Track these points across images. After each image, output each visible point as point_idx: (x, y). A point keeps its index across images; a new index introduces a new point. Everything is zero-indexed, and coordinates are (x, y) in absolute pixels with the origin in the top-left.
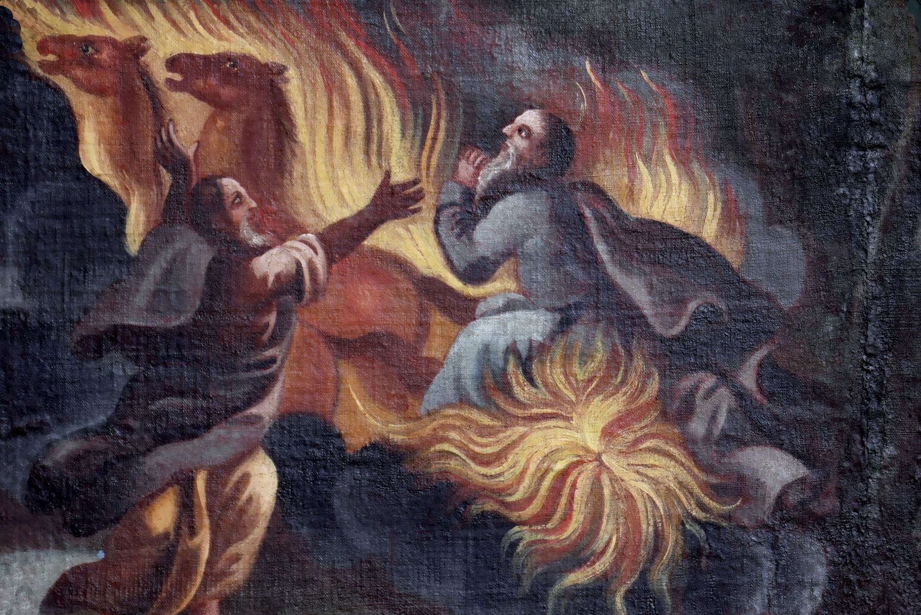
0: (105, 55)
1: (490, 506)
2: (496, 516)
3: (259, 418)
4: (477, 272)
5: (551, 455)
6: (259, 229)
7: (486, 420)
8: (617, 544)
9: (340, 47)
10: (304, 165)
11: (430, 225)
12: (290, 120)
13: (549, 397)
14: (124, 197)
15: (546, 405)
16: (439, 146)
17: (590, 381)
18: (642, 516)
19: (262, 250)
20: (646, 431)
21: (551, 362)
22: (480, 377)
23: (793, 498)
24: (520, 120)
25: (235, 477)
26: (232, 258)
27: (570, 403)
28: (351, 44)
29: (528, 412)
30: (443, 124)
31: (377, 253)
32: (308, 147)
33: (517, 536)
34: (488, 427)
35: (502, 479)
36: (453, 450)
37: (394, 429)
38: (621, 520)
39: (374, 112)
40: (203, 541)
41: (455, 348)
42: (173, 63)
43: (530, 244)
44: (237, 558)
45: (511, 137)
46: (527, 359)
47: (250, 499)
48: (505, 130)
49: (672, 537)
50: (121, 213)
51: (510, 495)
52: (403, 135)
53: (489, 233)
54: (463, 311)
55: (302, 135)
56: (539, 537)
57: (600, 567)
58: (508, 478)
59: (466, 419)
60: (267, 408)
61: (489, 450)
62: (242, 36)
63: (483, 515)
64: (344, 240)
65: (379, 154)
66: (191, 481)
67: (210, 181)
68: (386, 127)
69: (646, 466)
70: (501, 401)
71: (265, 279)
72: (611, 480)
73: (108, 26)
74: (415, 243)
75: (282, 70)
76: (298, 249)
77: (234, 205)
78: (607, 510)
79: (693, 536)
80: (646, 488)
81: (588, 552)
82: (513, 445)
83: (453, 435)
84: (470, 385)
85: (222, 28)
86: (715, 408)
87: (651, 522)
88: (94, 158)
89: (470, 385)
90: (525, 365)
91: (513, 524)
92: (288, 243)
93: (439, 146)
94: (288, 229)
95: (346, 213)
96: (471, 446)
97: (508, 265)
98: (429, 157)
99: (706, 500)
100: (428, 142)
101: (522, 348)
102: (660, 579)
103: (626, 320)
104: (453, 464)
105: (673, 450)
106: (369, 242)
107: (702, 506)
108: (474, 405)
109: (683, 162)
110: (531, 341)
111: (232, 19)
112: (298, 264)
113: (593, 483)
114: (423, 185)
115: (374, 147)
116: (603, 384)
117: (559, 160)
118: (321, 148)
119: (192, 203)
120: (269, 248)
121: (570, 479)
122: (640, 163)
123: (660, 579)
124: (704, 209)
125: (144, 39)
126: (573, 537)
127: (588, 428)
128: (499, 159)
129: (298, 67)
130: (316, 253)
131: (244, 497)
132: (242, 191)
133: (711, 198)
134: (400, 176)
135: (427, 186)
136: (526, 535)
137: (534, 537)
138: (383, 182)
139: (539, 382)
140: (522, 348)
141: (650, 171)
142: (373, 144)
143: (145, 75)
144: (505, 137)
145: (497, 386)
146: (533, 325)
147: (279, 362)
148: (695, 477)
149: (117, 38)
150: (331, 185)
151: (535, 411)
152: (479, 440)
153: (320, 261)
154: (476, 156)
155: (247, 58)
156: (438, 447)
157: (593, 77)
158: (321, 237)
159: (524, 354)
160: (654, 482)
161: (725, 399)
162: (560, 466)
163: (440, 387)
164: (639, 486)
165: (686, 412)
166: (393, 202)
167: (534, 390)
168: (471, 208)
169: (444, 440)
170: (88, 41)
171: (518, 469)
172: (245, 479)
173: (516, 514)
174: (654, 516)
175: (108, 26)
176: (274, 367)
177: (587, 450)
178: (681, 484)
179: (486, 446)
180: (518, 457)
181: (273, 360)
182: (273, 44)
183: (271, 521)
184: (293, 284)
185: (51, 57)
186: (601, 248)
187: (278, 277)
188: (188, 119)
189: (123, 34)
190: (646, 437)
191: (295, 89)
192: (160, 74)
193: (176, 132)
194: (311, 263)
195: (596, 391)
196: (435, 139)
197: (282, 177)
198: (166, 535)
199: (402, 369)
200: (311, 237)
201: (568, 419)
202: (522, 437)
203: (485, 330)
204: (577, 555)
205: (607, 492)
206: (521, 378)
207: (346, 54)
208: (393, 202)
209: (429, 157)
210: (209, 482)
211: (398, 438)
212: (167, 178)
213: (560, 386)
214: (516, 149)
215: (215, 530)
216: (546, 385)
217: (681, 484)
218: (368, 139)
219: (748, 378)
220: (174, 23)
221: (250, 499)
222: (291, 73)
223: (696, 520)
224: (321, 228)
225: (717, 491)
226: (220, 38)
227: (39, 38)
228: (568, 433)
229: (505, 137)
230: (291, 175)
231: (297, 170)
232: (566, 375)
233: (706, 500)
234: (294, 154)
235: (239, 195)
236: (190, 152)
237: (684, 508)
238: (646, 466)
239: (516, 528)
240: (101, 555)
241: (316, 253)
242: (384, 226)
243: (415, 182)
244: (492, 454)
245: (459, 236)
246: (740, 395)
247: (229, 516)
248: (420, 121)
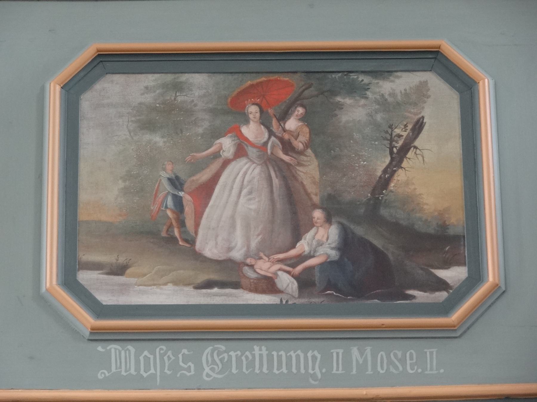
128: (251, 116)
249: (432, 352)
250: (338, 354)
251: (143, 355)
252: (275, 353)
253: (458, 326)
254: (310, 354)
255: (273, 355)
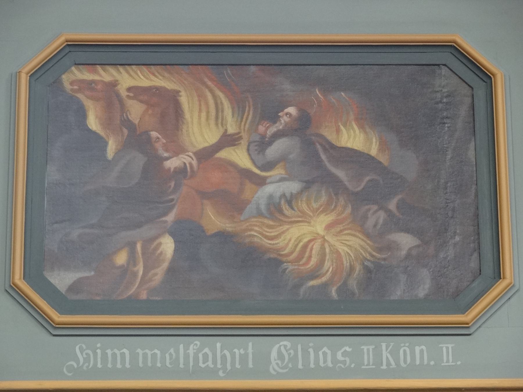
0: (99, 87)
1: (272, 256)
2: (275, 259)
3: (166, 222)
4: (269, 166)
5: (299, 240)
6: (167, 151)
7: (271, 223)
8: (332, 270)
9: (204, 84)
10: (188, 127)
11: (245, 151)
12: (182, 111)
13: (300, 214)
14: (107, 140)
15: (300, 217)
16: (249, 121)
17: (318, 209)
18: (344, 260)
19: (167, 159)
20: (346, 227)
21: (301, 201)
22: (268, 205)
23: (414, 252)
24: (286, 110)
25: (155, 243)
26: (155, 162)
27: (310, 216)
28: (209, 83)
29: (290, 220)
30: (251, 113)
31: (220, 159)
32: (189, 120)
33: (286, 267)
34: (272, 225)
35: (278, 245)
36: (255, 234)
37: (228, 226)
38: (334, 261)
39: (220, 107)
40: (140, 269)
41: (257, 195)
42: (129, 89)
43: (291, 156)
44: (156, 274)
45: (282, 117)
46: (291, 200)
47: (161, 253)
48: (279, 114)
49: (358, 267)
50: (106, 143)
51: (283, 251)
52: (233, 116)
53: (274, 151)
54: (261, 182)
55: (187, 115)
56: (296, 267)
57: (324, 279)
58: (282, 244)
59: (262, 222)
60: (170, 218)
61: (272, 234)
62: (160, 80)
63: (269, 259)
64: (206, 155)
65: (222, 124)
66: (135, 243)
67: (147, 133)
68: (225, 113)
69: (347, 240)
70: (277, 215)
71: (169, 169)
72: (329, 246)
73: (101, 76)
74: (239, 157)
75: (178, 92)
76: (184, 158)
77: (155, 142)
78: (327, 257)
79: (367, 266)
80: (346, 249)
81: (319, 273)
82: (283, 232)
83: (256, 228)
84: (263, 207)
85: (153, 78)
86: (377, 217)
87: (348, 261)
88: (93, 123)
89: (263, 207)
90: (289, 203)
91: (284, 262)
92: (181, 156)
93: (249, 121)
94: (179, 150)
95: (206, 145)
96: (264, 233)
97: (282, 164)
98: (245, 125)
99: (374, 253)
100: (244, 120)
101: (288, 195)
102: (353, 284)
103: (335, 185)
104: (256, 239)
105: (358, 234)
106: (218, 155)
107: (373, 256)
108: (266, 217)
109: (361, 127)
110: (292, 193)
111: (157, 74)
112: (185, 164)
113: (321, 248)
114: (242, 134)
115: (220, 121)
116: (326, 209)
117: (303, 126)
118: (195, 120)
119: (136, 139)
120: (172, 157)
121: (310, 246)
122: (342, 127)
123: (353, 284)
124: (371, 143)
125: (117, 81)
126: (312, 268)
127: (319, 225)
128: (277, 125)
129: (186, 91)
130: (193, 159)
131: (159, 252)
132: (160, 136)
133: (374, 140)
134: (231, 130)
135: (244, 135)
136: (291, 267)
137: (293, 267)
138: (224, 133)
139: (296, 208)
140: (288, 195)
141: (346, 130)
142: (219, 119)
143: (118, 95)
144: (280, 117)
145: (275, 210)
146: (293, 187)
147: (175, 201)
148: (368, 244)
149: (104, 80)
150: (200, 132)
151: (293, 219)
152: (268, 230)
153: (195, 163)
154: (266, 124)
155: (164, 88)
156: (249, 233)
157: (320, 95)
158: (195, 154)
159: (289, 199)
160: (349, 246)
161: (382, 215)
162: (306, 240)
163: (250, 209)
164: (342, 249)
165: (365, 218)
166: (228, 141)
167: (293, 212)
168: (263, 144)
169: (251, 230)
170: (93, 81)
171: (286, 242)
172: (160, 244)
173: (285, 259)
174: (349, 259)
175: (101, 76)
176: (173, 203)
177: (318, 234)
178: (361, 246)
179: (271, 232)
180: (288, 236)
181: (172, 200)
182: (175, 83)
183: (170, 263)
184: (182, 172)
185: (76, 87)
186: (323, 157)
187: (175, 168)
188: (136, 110)
189: (107, 78)
190: (345, 229)
191: (184, 99)
192: (124, 93)
193: (130, 114)
194: (191, 164)
195: (322, 212)
196: (247, 119)
197: (178, 130)
198: (122, 266)
199: (233, 204)
200: (191, 154)
201: (309, 223)
202: (288, 229)
203: (269, 189)
204: (314, 274)
205: (327, 250)
206: (287, 207)
207: (208, 87)
208: (228, 141)
209: (245, 125)
210: (143, 248)
211: (230, 229)
212: (126, 131)
213: (306, 210)
214: (285, 121)
215: (145, 267)
216: (299, 211)
217: (361, 246)
218: (217, 118)
219: (392, 205)
220: (130, 75)
221: (161, 253)
222: (183, 93)
223: (369, 260)
224: (195, 150)
225: (380, 250)
226: (151, 80)
227: (70, 81)
228: (309, 228)
229: (280, 117)
230: (182, 131)
231: (185, 128)
232: (308, 207)
233: (374, 253)
234: (183, 123)
235: (158, 138)
236: (136, 122)
237: (363, 256)
238: (347, 240)
239: (285, 264)
240: (93, 273)
241: (193, 159)
242: (224, 150)
243: (239, 133)
244: (274, 236)
245: (259, 153)
246: (389, 212)
247: (152, 258)
248: (241, 109)
249: (447, 347)
250: (447, 348)
251: (323, 350)
252: (109, 352)
253: (472, 323)
254: (417, 349)
255: (107, 353)
